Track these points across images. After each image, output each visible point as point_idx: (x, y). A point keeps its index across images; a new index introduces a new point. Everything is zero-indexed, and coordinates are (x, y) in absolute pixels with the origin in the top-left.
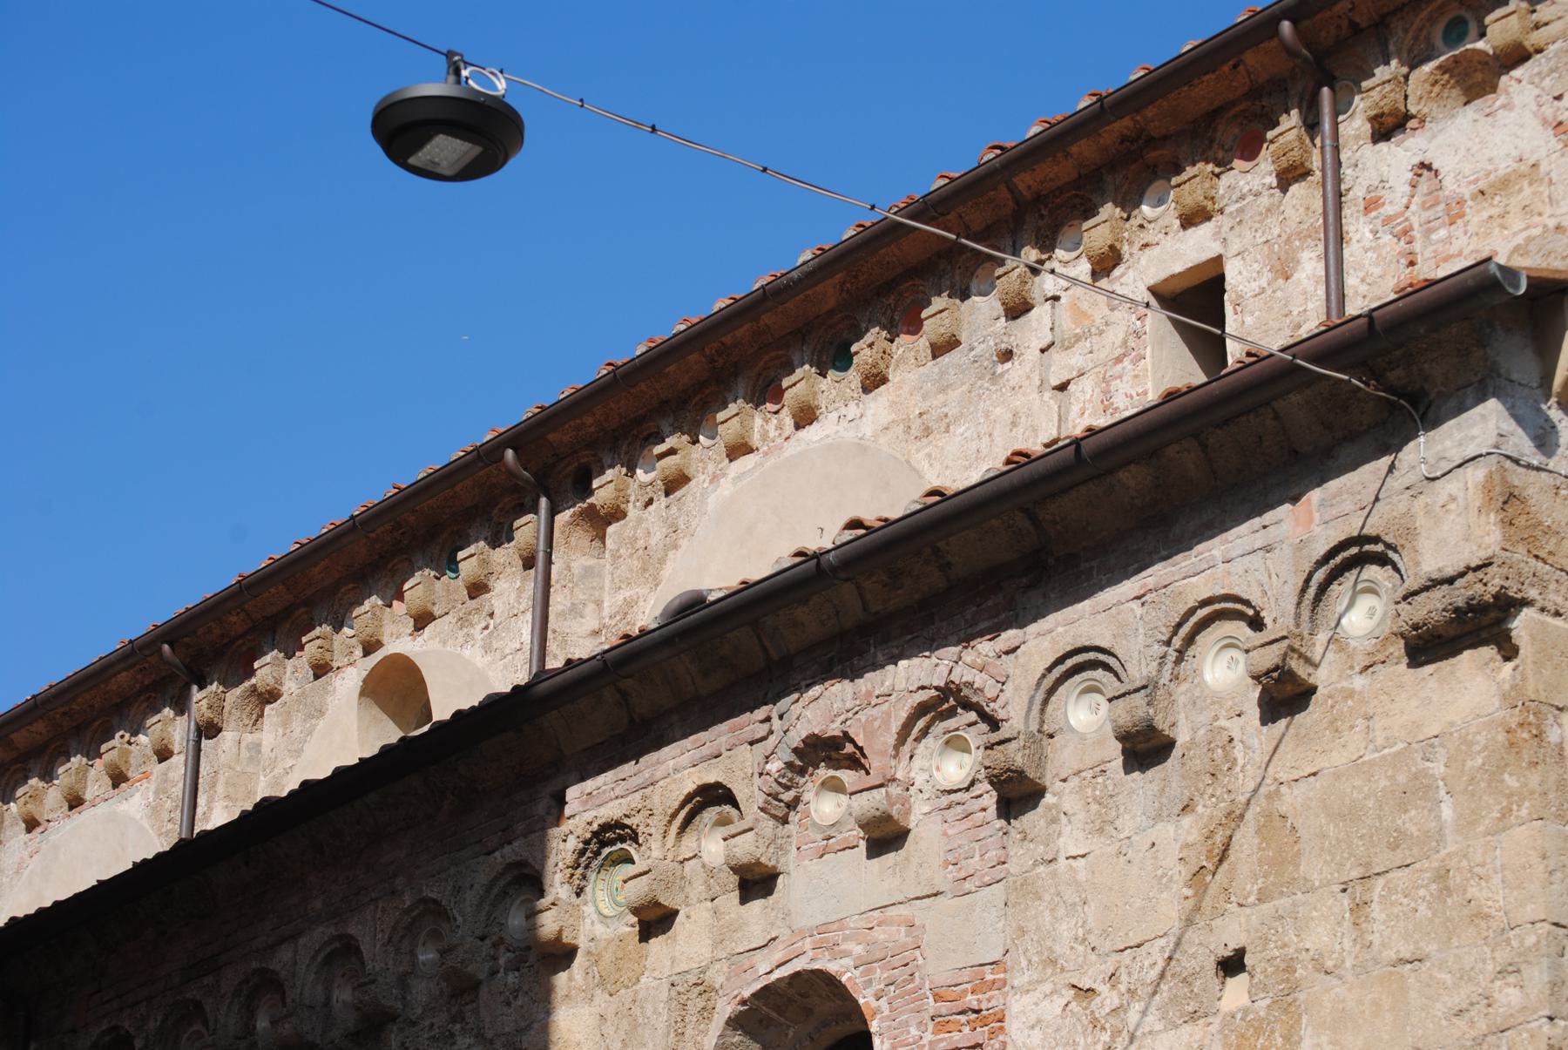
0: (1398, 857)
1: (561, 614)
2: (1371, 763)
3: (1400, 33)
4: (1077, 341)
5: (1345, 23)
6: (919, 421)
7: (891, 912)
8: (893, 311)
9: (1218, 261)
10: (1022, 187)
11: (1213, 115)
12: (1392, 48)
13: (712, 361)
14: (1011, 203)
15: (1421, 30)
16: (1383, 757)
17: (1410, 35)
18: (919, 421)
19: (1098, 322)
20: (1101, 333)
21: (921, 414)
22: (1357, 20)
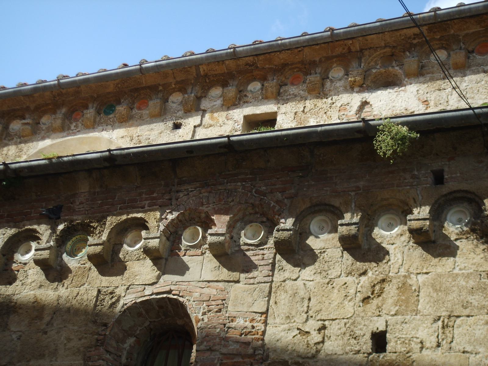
0: (467, 312)
1: (454, 22)
2: (457, 275)
3: (367, 57)
4: (210, 126)
5: (347, 48)
6: (137, 138)
7: (211, 284)
8: (135, 99)
9: (276, 113)
10: (201, 70)
11: (284, 66)
12: (363, 60)
13: (54, 97)
14: (194, 74)
15: (375, 57)
16: (463, 273)
17: (371, 58)
18: (137, 138)
19: (221, 122)
20: (221, 126)
21: (138, 136)
22: (352, 48)
